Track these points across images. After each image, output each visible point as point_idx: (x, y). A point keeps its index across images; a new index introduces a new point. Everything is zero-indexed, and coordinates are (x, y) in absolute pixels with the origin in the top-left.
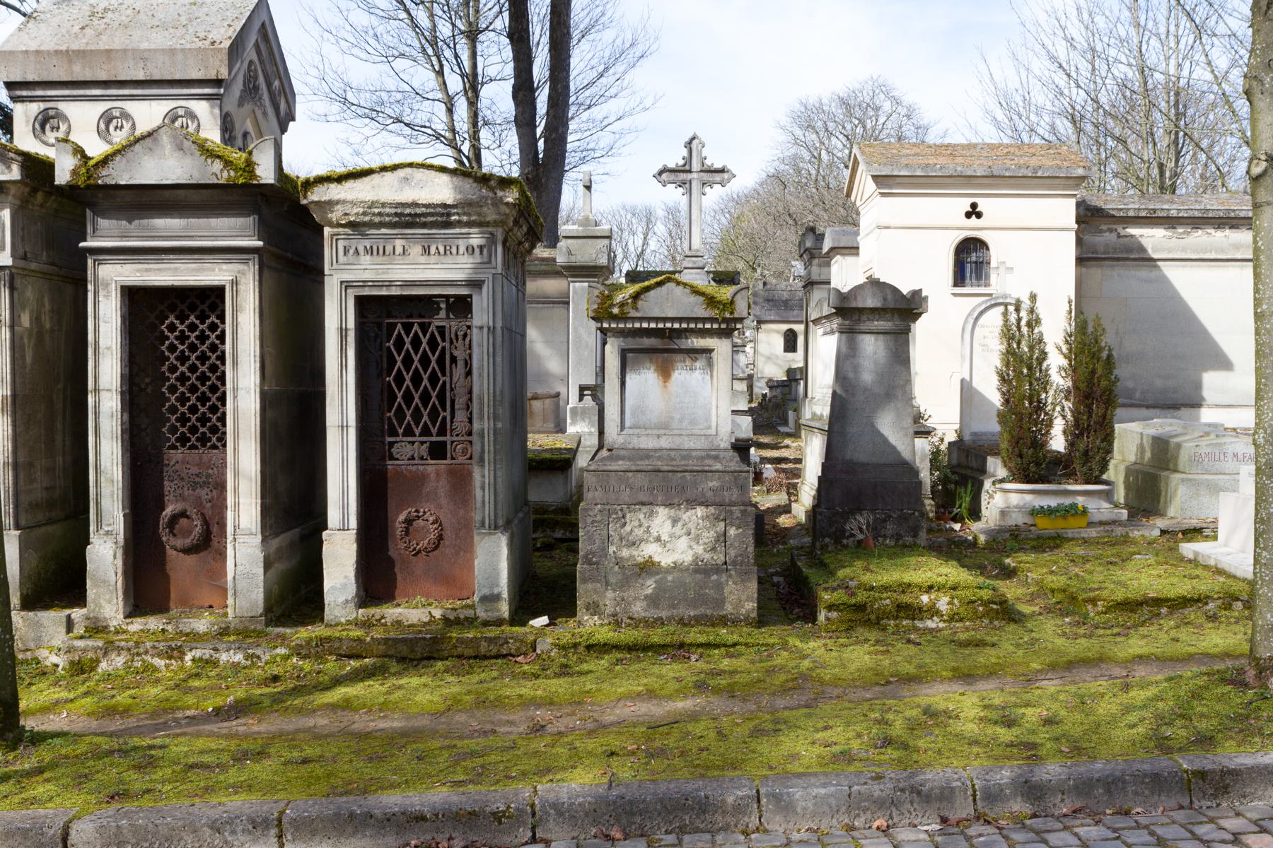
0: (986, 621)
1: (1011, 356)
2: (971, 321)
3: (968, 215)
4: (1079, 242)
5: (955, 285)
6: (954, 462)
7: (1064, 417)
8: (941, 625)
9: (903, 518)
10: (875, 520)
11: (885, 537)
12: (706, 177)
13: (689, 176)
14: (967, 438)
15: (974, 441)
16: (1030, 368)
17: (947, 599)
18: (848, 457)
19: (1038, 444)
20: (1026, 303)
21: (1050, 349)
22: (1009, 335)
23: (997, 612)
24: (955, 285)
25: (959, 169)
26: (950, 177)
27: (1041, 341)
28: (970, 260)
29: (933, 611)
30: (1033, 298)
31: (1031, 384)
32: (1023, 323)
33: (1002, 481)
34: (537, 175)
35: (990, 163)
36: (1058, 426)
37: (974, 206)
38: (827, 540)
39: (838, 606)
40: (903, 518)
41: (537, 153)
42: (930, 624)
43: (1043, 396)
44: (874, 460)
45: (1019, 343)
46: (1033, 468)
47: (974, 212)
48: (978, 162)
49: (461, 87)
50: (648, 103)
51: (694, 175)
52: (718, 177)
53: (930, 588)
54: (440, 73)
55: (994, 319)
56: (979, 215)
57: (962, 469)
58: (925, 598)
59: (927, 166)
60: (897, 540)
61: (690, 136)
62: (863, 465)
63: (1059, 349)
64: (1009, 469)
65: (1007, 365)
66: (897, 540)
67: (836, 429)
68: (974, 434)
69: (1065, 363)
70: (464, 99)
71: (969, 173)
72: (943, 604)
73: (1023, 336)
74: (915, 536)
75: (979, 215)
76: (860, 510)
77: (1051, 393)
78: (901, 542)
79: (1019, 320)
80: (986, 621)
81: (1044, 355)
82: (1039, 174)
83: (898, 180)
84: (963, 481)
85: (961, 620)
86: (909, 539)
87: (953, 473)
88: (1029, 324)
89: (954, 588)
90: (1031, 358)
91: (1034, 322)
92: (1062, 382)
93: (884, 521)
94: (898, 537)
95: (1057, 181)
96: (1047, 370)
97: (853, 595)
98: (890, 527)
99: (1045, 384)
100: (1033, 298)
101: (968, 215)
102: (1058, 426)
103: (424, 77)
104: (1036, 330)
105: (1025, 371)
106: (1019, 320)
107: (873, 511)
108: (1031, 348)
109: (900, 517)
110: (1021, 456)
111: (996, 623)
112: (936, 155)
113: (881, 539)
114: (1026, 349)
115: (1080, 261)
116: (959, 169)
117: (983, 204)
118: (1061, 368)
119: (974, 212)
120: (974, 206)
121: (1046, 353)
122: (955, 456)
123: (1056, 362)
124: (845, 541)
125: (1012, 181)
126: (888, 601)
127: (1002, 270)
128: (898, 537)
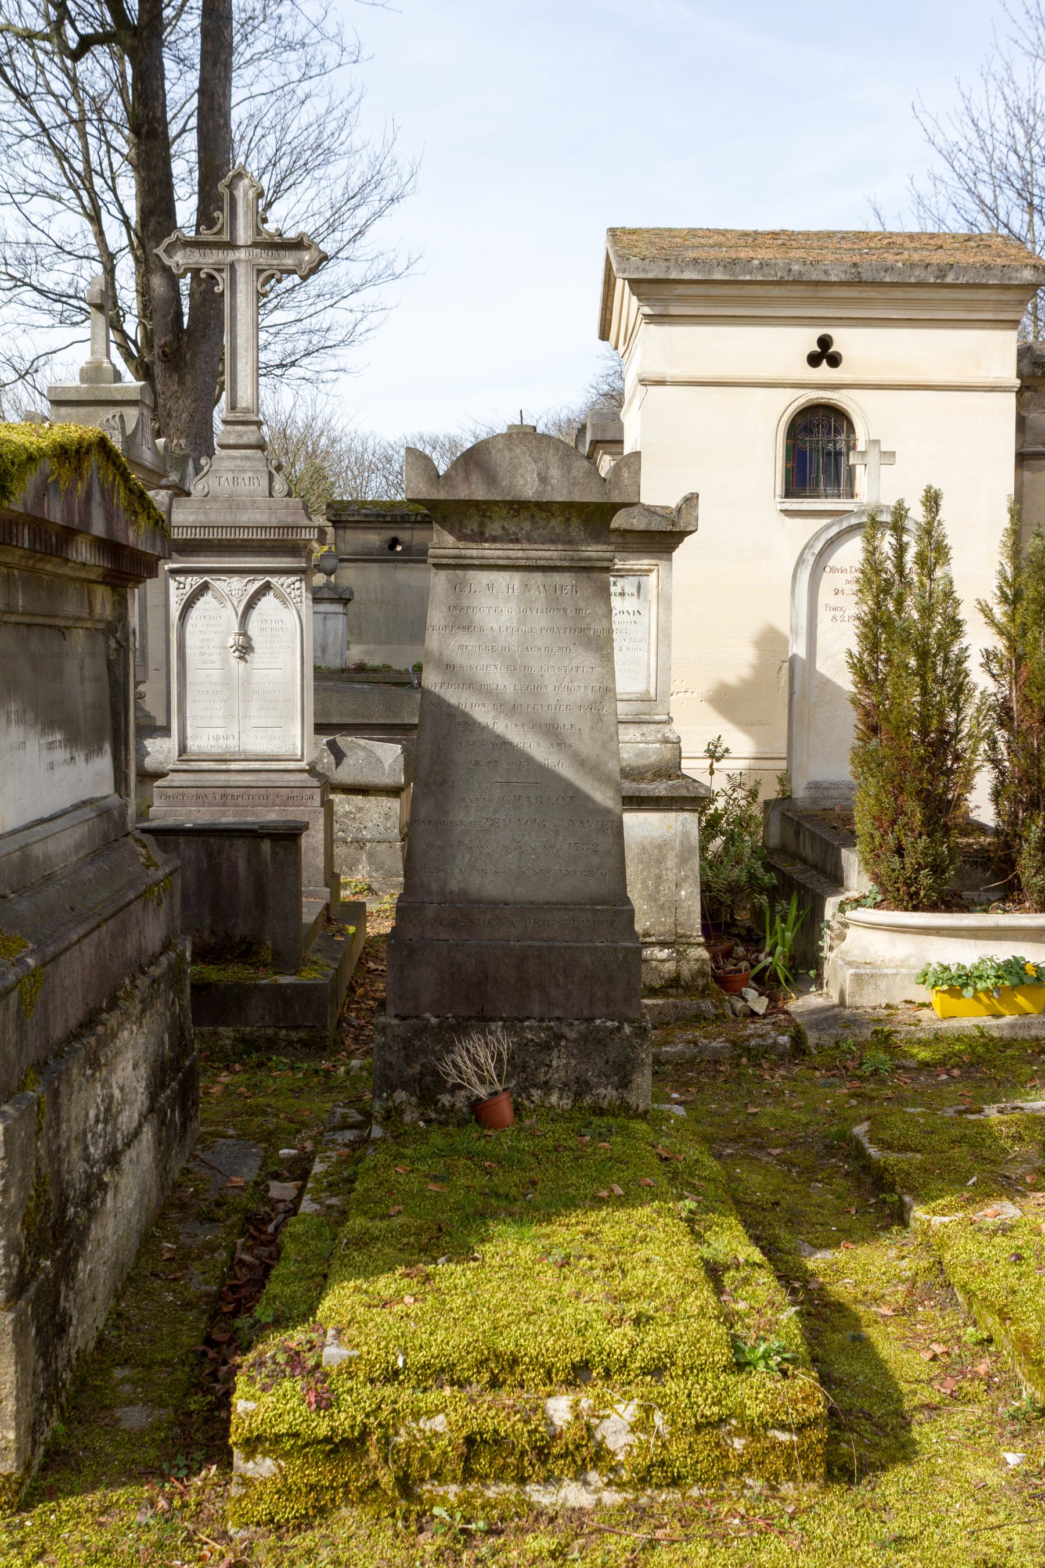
0: (756, 1484)
1: (878, 629)
2: (811, 560)
3: (814, 360)
4: (1021, 424)
5: (789, 493)
6: (774, 842)
7: (996, 763)
8: (612, 1498)
9: (593, 1041)
10: (523, 1046)
11: (547, 1087)
12: (263, 258)
13: (231, 256)
14: (800, 792)
15: (815, 801)
16: (923, 655)
17: (628, 1411)
18: (454, 885)
19: (941, 811)
20: (917, 513)
21: (968, 613)
22: (880, 585)
23: (787, 1453)
24: (789, 493)
25: (796, 268)
26: (780, 283)
27: (948, 594)
28: (816, 448)
29: (586, 1455)
30: (932, 501)
31: (925, 691)
32: (910, 556)
33: (858, 903)
34: (179, 348)
35: (857, 259)
36: (984, 780)
37: (825, 342)
38: (400, 1096)
39: (278, 1438)
40: (593, 1041)
41: (179, 314)
42: (573, 1495)
43: (952, 718)
44: (521, 892)
45: (900, 602)
46: (925, 879)
47: (824, 354)
48: (831, 257)
49: (125, 242)
50: (399, 268)
51: (242, 254)
52: (289, 260)
53: (579, 1373)
54: (95, 218)
55: (851, 553)
56: (835, 361)
57: (771, 880)
58: (560, 1408)
59: (734, 262)
60: (578, 1096)
61: (789, 521)
62: (493, 904)
63: (986, 611)
64: (876, 878)
65: (874, 648)
66: (578, 1096)
67: (422, 814)
68: (815, 786)
69: (999, 644)
70: (130, 256)
71: (814, 277)
72: (617, 1431)
73: (909, 584)
74: (624, 1084)
75: (835, 361)
76: (483, 1020)
77: (970, 711)
78: (588, 1100)
79: (901, 550)
80: (756, 1484)
81: (955, 626)
82: (949, 279)
83: (681, 290)
84: (785, 888)
85: (675, 1482)
86: (607, 1094)
87: (768, 867)
88: (921, 559)
89: (656, 1370)
90: (925, 634)
91: (935, 551)
92: (991, 686)
93: (546, 1047)
94: (580, 1088)
95: (983, 294)
96: (960, 663)
97: (325, 1403)
98: (560, 1064)
99: (959, 690)
100: (932, 501)
101: (814, 360)
102: (984, 780)
103: (71, 224)
104: (939, 573)
105: (913, 662)
106: (901, 550)
107: (512, 1024)
108: (927, 612)
109: (584, 1037)
110: (900, 851)
111: (787, 1489)
112: (755, 247)
113: (536, 1094)
114: (916, 616)
115: (1022, 458)
116: (796, 268)
117: (843, 339)
118: (989, 656)
119: (824, 354)
120: (825, 342)
121: (958, 624)
122: (775, 828)
123: (979, 639)
124: (446, 1099)
125: (898, 293)
126: (439, 1423)
127: (873, 458)
128: (580, 1088)
